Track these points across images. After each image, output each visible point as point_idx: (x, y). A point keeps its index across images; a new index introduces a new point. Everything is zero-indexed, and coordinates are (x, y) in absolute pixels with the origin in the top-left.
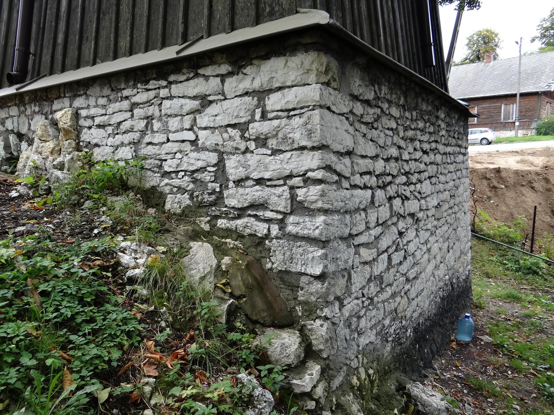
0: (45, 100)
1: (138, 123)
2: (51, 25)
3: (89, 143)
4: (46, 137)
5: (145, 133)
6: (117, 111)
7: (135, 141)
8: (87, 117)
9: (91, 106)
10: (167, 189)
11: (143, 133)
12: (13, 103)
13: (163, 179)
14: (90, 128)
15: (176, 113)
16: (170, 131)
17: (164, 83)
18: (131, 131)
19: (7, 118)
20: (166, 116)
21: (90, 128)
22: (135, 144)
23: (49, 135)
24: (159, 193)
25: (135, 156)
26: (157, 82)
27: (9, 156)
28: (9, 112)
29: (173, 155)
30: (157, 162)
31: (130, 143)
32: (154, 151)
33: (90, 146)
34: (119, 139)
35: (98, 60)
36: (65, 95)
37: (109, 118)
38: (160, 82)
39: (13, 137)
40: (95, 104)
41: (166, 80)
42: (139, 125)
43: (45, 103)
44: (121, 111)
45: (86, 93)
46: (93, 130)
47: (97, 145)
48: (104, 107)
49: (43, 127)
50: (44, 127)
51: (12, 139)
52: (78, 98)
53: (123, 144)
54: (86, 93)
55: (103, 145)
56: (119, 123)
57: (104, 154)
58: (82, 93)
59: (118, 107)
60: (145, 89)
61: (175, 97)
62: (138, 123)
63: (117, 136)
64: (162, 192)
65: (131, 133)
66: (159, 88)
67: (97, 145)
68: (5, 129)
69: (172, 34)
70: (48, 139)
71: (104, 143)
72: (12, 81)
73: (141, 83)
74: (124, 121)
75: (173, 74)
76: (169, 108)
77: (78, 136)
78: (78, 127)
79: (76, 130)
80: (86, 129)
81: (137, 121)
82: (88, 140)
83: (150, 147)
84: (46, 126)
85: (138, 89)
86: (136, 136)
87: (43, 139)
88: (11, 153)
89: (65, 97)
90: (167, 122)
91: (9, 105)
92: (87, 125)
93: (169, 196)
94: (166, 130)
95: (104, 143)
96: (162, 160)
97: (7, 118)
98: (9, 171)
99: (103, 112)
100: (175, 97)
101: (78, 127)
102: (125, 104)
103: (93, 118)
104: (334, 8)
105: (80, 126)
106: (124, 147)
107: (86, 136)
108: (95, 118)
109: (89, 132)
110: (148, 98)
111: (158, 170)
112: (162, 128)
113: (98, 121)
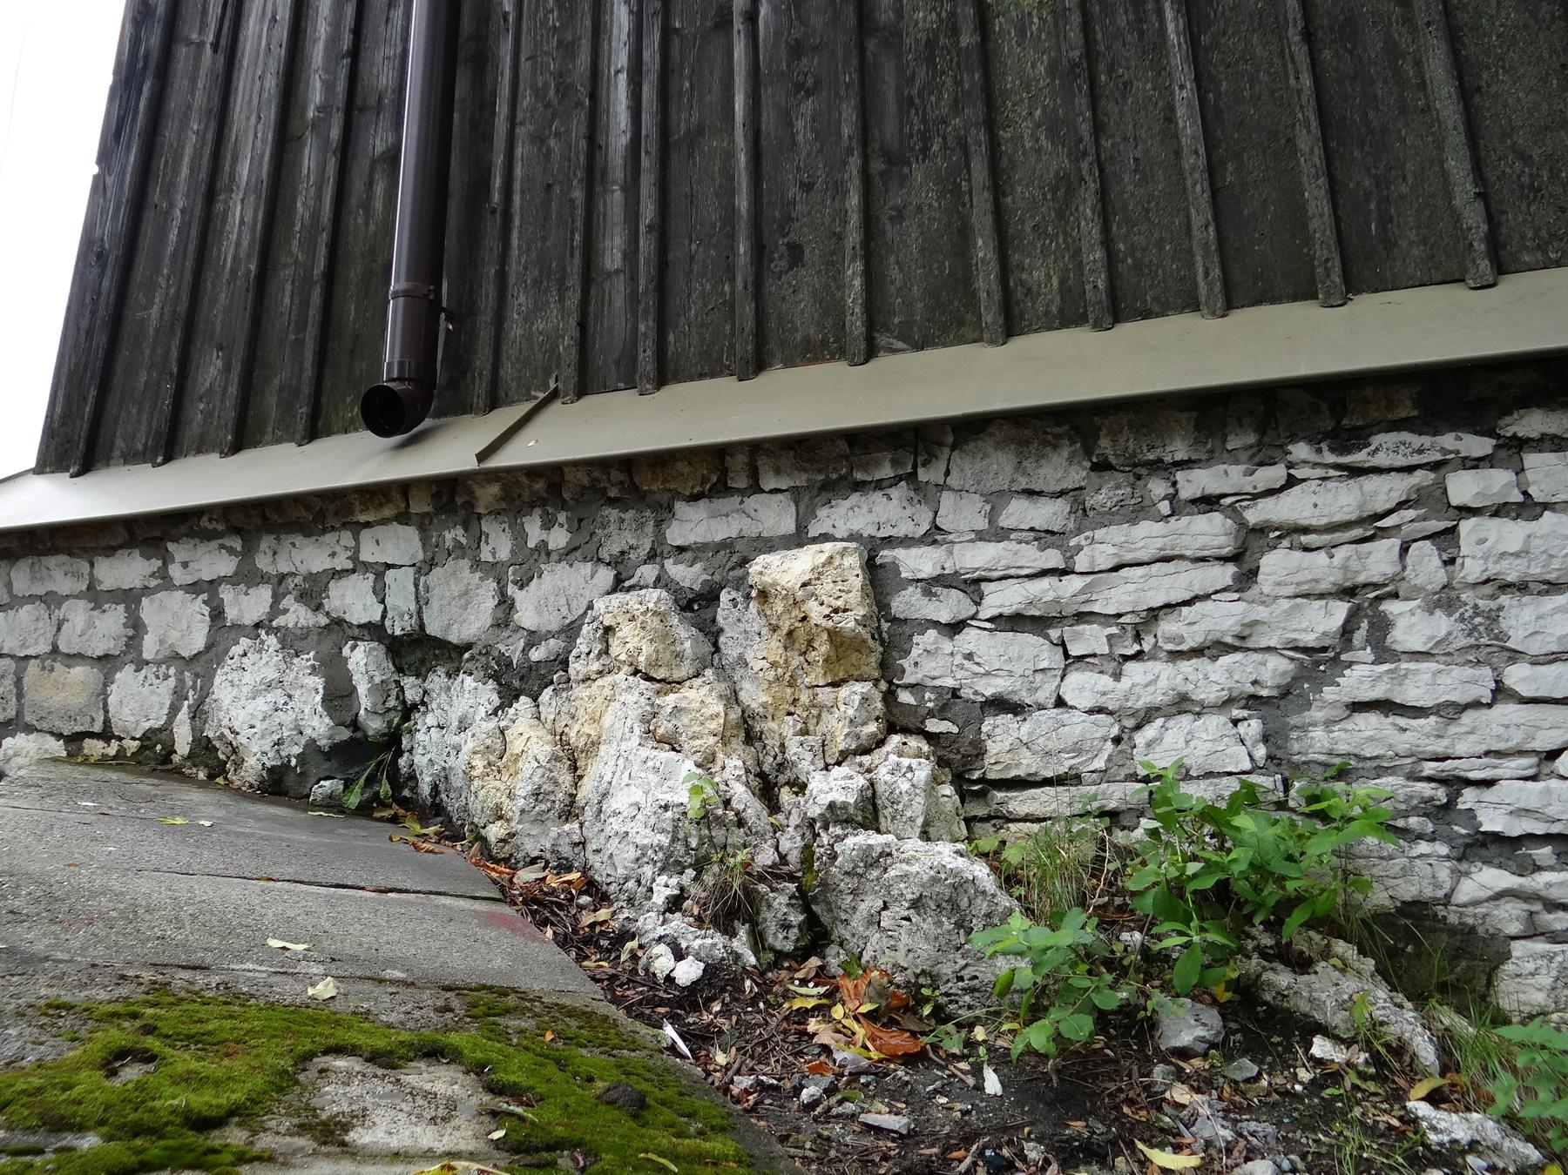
0: (612, 502)
1: (1289, 613)
2: (315, 216)
3: (955, 693)
4: (669, 666)
5: (1335, 660)
6: (1150, 554)
7: (1265, 693)
8: (933, 585)
9: (980, 540)
10: (1509, 918)
11: (1319, 662)
12: (388, 512)
13: (1464, 866)
14: (955, 628)
15: (1552, 577)
16: (1515, 656)
17: (1480, 446)
18: (1235, 649)
19: (337, 574)
20: (1488, 589)
21: (955, 628)
22: (1269, 708)
23: (679, 656)
24: (1452, 931)
25: (1270, 757)
26: (1426, 440)
27: (345, 734)
28: (357, 549)
29: (1533, 760)
30: (1426, 789)
31: (1229, 702)
32: (1403, 742)
33: (958, 706)
34: (1149, 681)
35: (882, 340)
36: (756, 481)
37: (1086, 589)
38: (1448, 440)
39: (368, 653)
40: (982, 524)
41: (1490, 433)
42: (1294, 624)
43: (612, 514)
44: (1166, 559)
45: (911, 477)
46: (970, 638)
47: (1001, 705)
48: (1045, 537)
49: (653, 623)
50: (656, 620)
51: (362, 660)
52: (855, 498)
53: (1182, 704)
54: (911, 477)
55: (1041, 707)
56: (1154, 614)
57: (1053, 745)
58: (886, 471)
59: (1159, 543)
60: (1337, 466)
61: (1546, 506)
62: (1289, 613)
63: (1130, 667)
64: (1473, 929)
65: (1238, 656)
66: (1436, 466)
67: (1001, 705)
68: (323, 621)
69: (1389, 244)
70: (677, 675)
71: (1041, 696)
72: (391, 415)
73: (1314, 441)
74: (1188, 603)
75: (1539, 406)
76: (1517, 555)
77: (888, 671)
78: (885, 626)
79: (879, 645)
80: (932, 634)
81: (1285, 604)
82: (949, 682)
83: (1370, 722)
84: (662, 617)
85: (1290, 466)
86: (1273, 671)
87: (661, 674)
88: (355, 725)
89: (756, 489)
90: (1493, 617)
91: (363, 518)
92: (945, 618)
93: (1518, 948)
94: (1491, 647)
95: (1045, 695)
96: (1456, 783)
97: (337, 574)
98: (353, 800)
99: (1053, 559)
100: (1546, 506)
101: (885, 626)
102: (1211, 531)
103: (973, 586)
104: (980, 243)
105: (894, 620)
106: (1185, 720)
107: (930, 663)
108: (986, 587)
109: (947, 646)
110: (1361, 506)
111: (1430, 827)
112: (1465, 642)
113: (1000, 599)
